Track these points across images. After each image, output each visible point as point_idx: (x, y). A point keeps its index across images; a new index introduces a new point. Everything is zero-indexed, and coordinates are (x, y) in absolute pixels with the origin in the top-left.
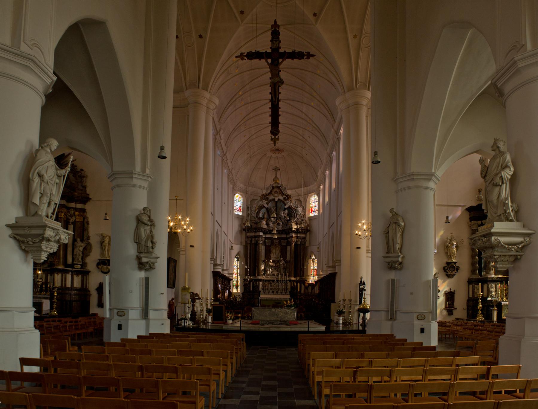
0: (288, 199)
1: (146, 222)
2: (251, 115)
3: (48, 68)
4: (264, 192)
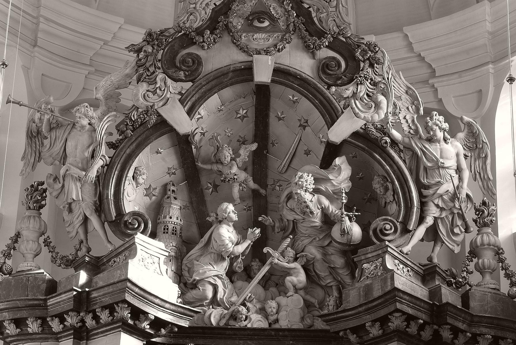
0: (352, 75)
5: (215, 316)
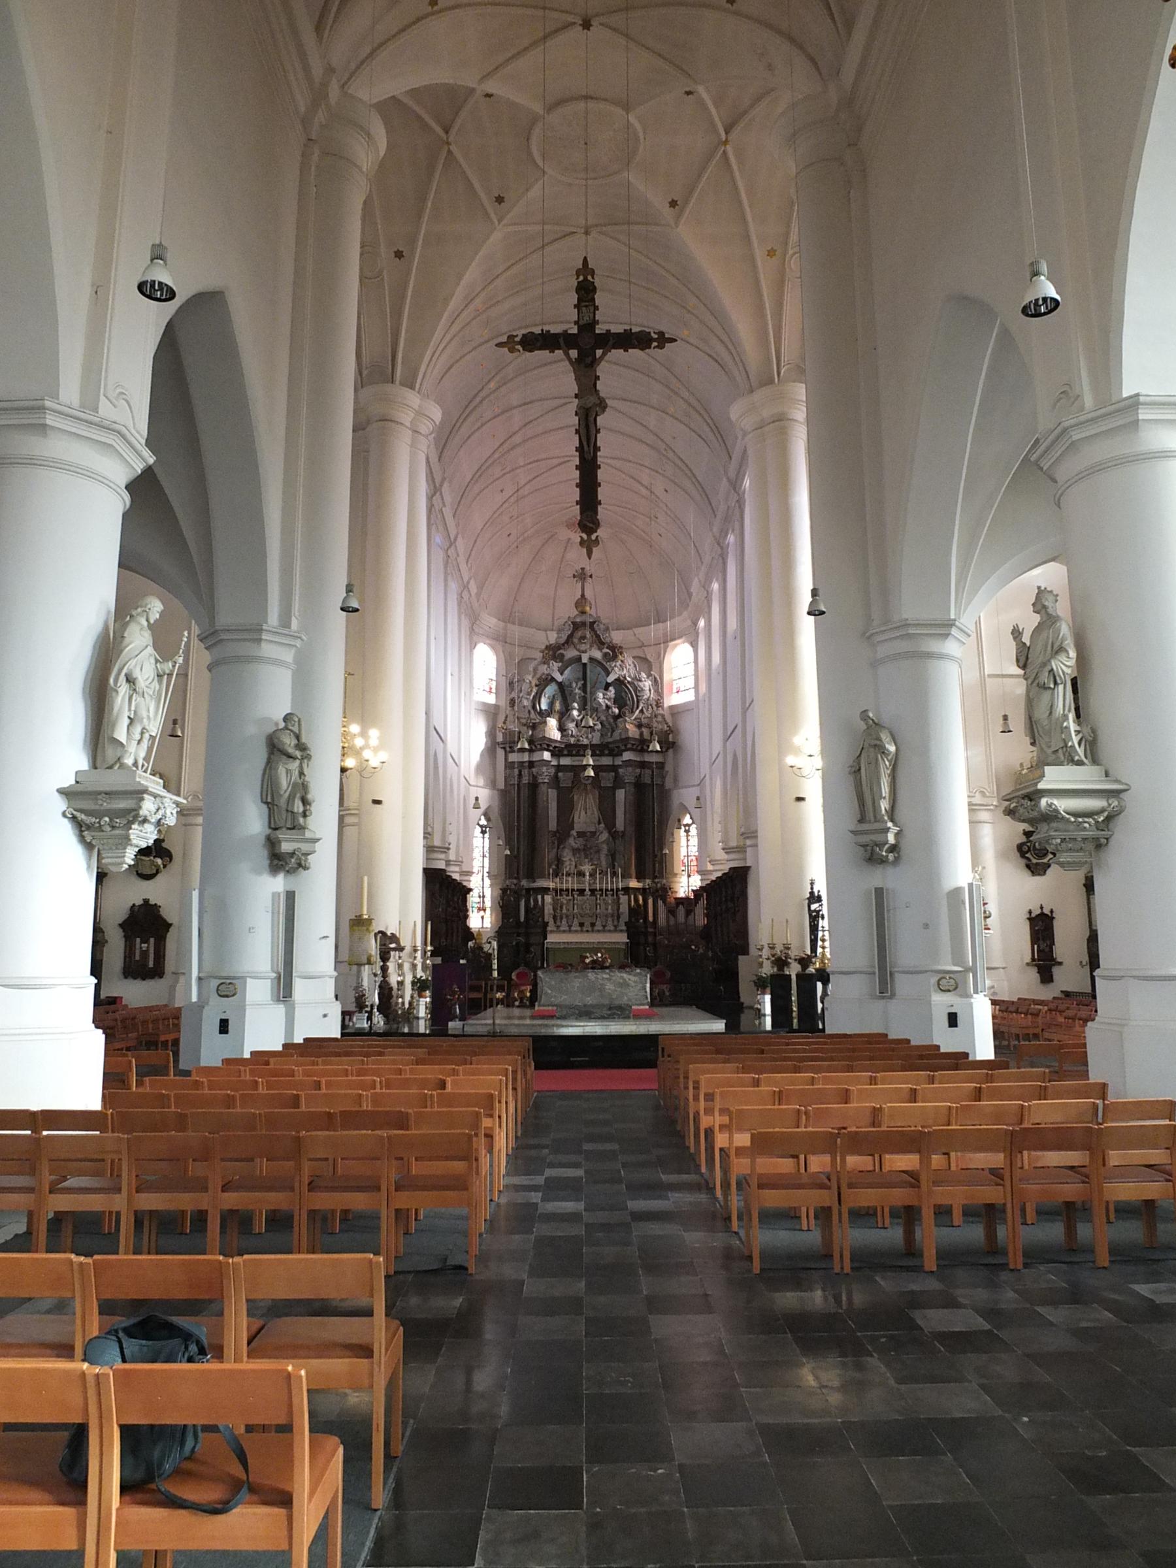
0: (615, 658)
1: (291, 750)
2: (517, 439)
3: (136, 435)
4: (553, 638)
5: (572, 740)
